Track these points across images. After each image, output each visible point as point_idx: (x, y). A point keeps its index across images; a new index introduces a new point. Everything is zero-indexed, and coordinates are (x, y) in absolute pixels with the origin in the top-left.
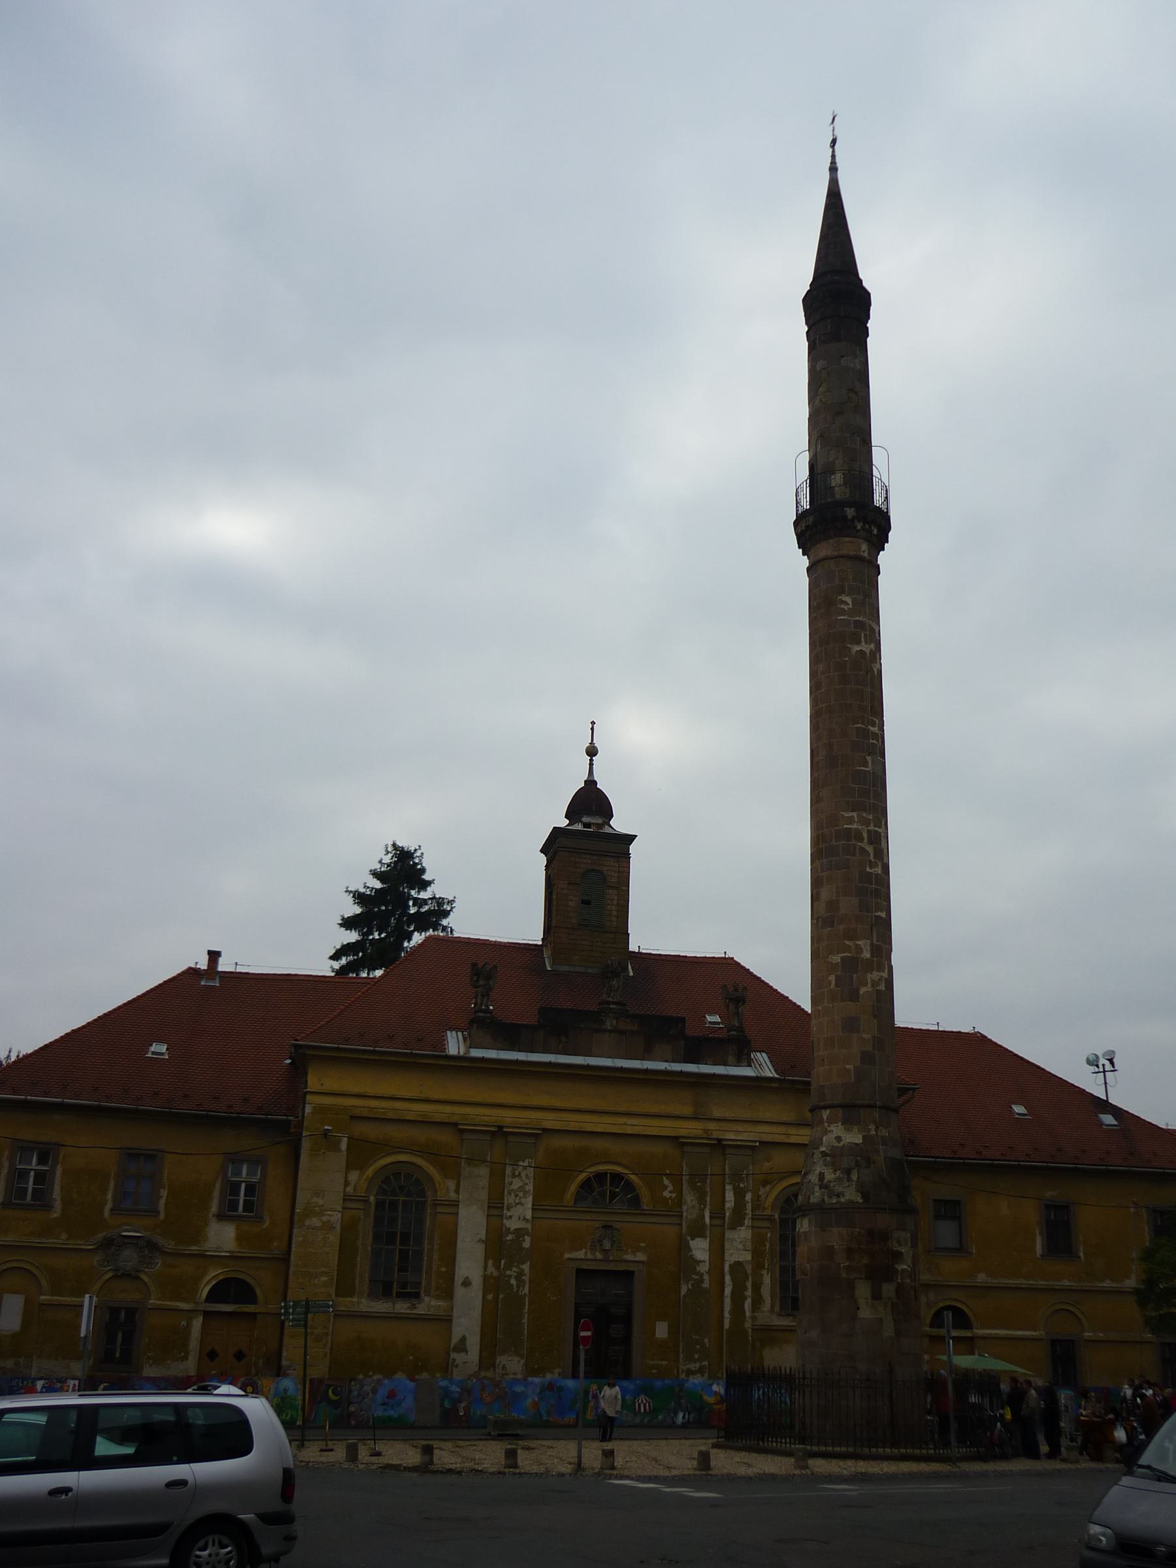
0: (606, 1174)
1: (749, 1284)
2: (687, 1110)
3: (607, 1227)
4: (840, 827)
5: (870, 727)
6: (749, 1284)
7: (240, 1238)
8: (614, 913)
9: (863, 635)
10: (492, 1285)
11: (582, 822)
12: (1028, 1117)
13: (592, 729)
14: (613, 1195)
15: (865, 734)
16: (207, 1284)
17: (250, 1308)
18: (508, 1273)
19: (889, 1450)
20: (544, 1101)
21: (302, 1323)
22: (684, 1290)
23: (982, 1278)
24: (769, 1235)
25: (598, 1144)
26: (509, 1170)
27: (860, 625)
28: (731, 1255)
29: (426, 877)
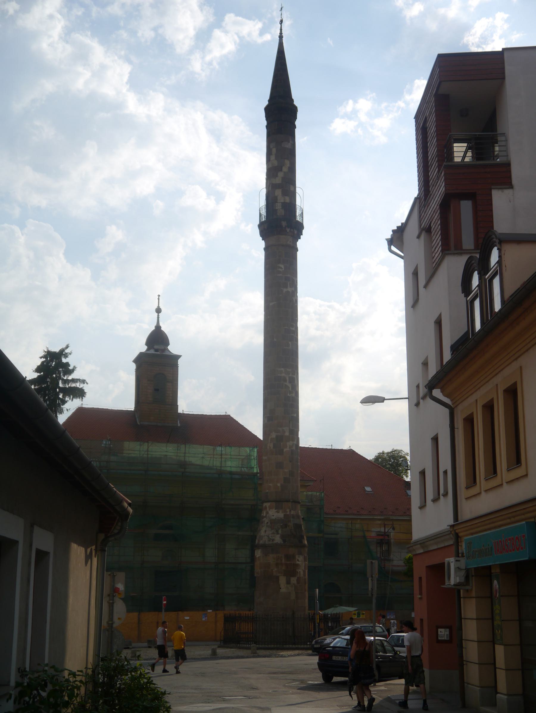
9: (289, 283)
11: (154, 348)
12: (372, 493)
13: (159, 299)
19: (291, 646)
29: (71, 368)
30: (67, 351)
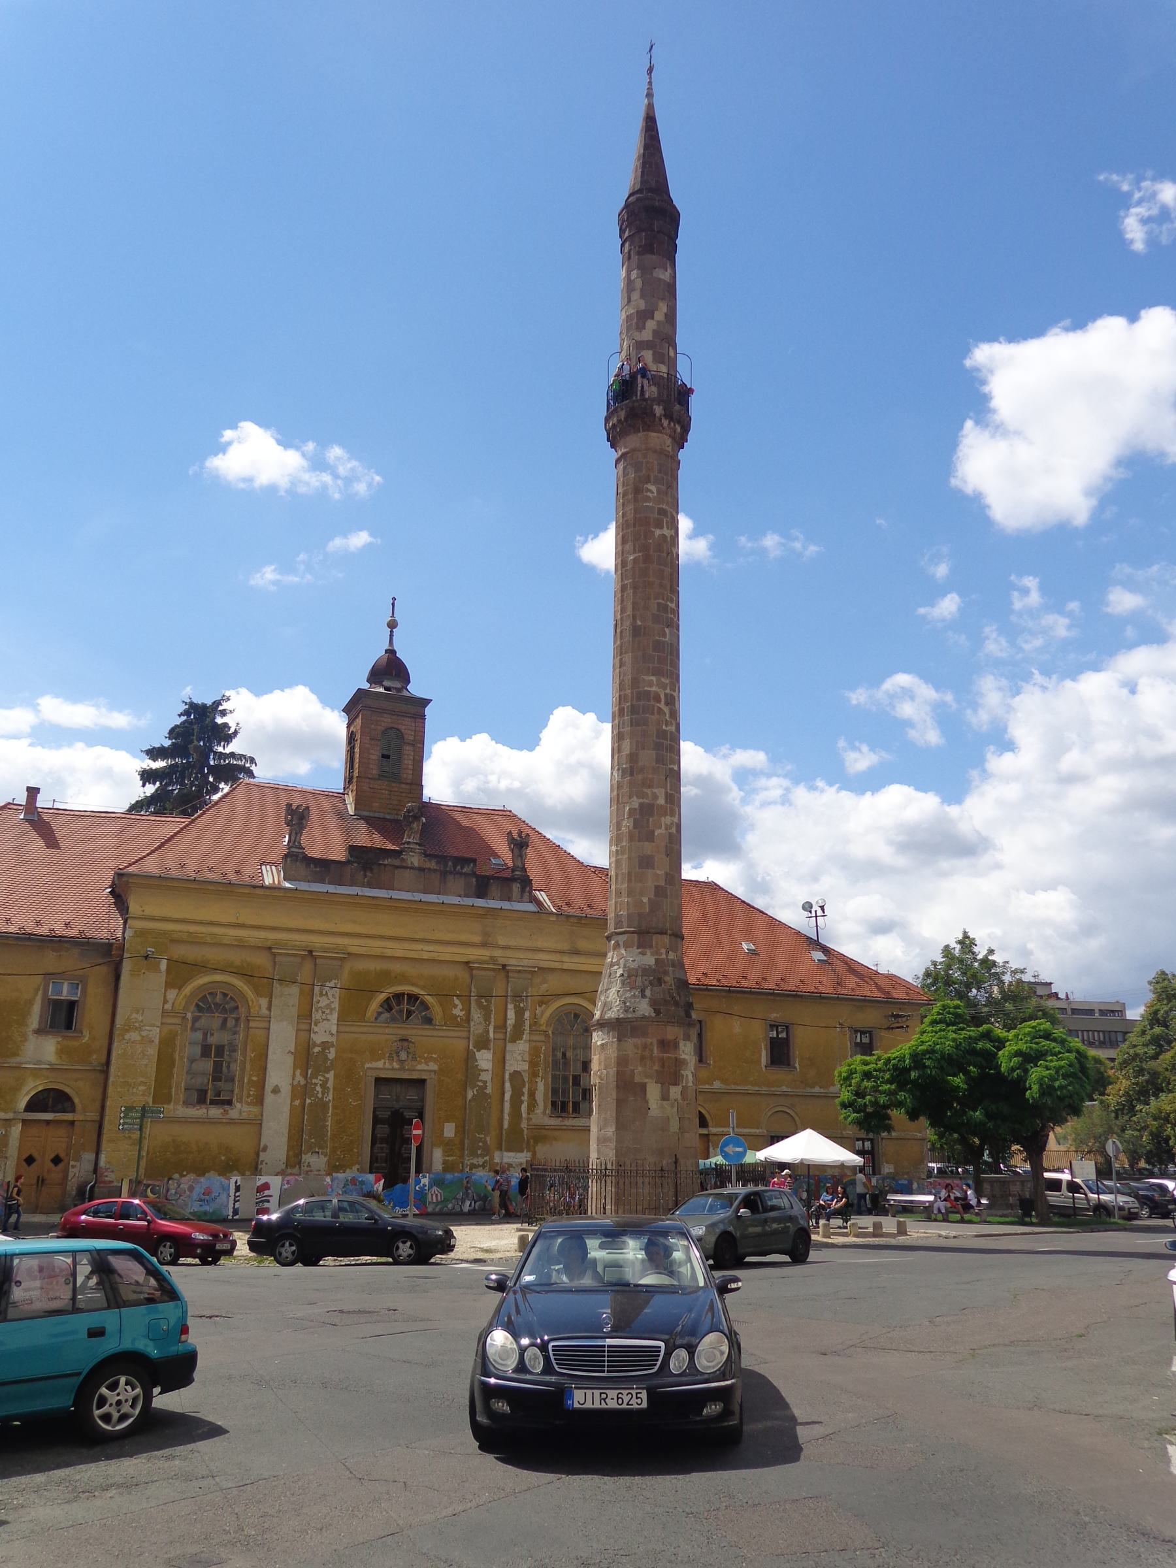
0: (403, 994)
1: (525, 1090)
2: (477, 939)
4: (641, 689)
5: (668, 603)
6: (525, 1090)
7: (61, 1052)
8: (411, 767)
10: (301, 1092)
13: (393, 604)
14: (409, 1013)
15: (665, 608)
16: (27, 1094)
17: (69, 1117)
18: (314, 1081)
20: (349, 928)
21: (136, 1127)
22: (470, 1094)
23: (717, 1084)
24: (544, 1048)
25: (397, 968)
26: (317, 989)
27: (662, 512)
28: (511, 1065)
30: (225, 706)
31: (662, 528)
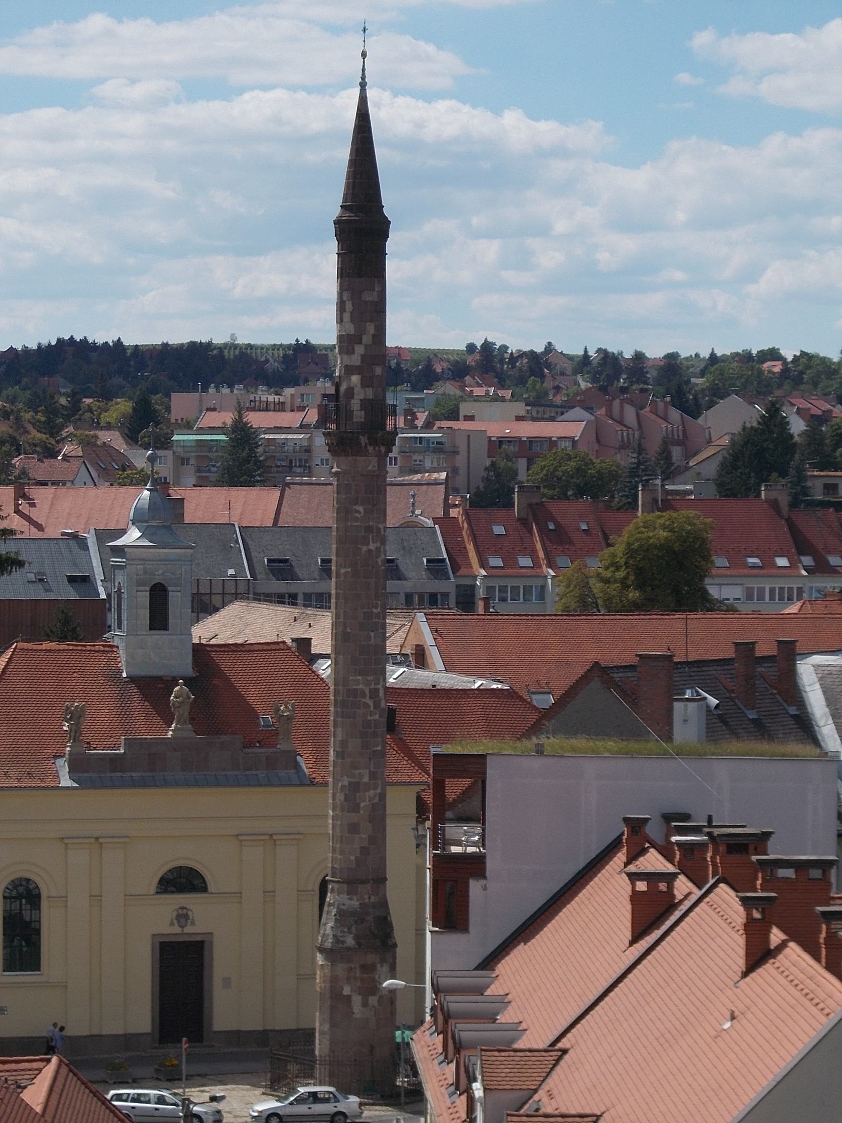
3: (183, 908)
27: (369, 529)
31: (368, 544)
